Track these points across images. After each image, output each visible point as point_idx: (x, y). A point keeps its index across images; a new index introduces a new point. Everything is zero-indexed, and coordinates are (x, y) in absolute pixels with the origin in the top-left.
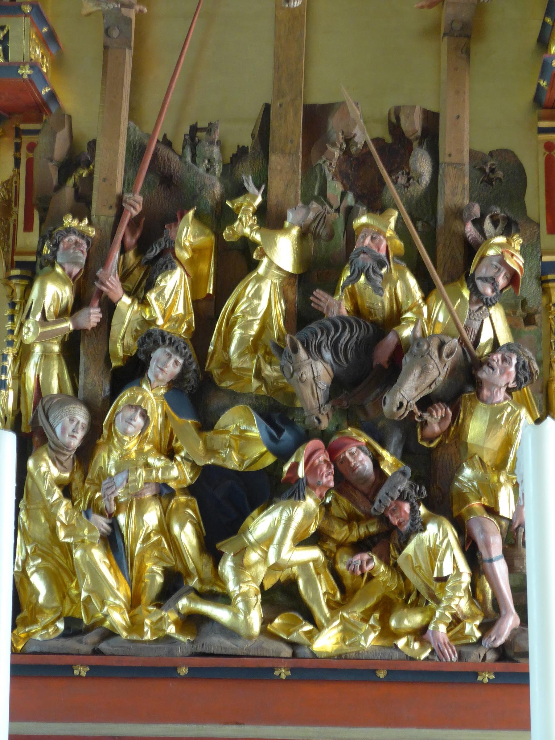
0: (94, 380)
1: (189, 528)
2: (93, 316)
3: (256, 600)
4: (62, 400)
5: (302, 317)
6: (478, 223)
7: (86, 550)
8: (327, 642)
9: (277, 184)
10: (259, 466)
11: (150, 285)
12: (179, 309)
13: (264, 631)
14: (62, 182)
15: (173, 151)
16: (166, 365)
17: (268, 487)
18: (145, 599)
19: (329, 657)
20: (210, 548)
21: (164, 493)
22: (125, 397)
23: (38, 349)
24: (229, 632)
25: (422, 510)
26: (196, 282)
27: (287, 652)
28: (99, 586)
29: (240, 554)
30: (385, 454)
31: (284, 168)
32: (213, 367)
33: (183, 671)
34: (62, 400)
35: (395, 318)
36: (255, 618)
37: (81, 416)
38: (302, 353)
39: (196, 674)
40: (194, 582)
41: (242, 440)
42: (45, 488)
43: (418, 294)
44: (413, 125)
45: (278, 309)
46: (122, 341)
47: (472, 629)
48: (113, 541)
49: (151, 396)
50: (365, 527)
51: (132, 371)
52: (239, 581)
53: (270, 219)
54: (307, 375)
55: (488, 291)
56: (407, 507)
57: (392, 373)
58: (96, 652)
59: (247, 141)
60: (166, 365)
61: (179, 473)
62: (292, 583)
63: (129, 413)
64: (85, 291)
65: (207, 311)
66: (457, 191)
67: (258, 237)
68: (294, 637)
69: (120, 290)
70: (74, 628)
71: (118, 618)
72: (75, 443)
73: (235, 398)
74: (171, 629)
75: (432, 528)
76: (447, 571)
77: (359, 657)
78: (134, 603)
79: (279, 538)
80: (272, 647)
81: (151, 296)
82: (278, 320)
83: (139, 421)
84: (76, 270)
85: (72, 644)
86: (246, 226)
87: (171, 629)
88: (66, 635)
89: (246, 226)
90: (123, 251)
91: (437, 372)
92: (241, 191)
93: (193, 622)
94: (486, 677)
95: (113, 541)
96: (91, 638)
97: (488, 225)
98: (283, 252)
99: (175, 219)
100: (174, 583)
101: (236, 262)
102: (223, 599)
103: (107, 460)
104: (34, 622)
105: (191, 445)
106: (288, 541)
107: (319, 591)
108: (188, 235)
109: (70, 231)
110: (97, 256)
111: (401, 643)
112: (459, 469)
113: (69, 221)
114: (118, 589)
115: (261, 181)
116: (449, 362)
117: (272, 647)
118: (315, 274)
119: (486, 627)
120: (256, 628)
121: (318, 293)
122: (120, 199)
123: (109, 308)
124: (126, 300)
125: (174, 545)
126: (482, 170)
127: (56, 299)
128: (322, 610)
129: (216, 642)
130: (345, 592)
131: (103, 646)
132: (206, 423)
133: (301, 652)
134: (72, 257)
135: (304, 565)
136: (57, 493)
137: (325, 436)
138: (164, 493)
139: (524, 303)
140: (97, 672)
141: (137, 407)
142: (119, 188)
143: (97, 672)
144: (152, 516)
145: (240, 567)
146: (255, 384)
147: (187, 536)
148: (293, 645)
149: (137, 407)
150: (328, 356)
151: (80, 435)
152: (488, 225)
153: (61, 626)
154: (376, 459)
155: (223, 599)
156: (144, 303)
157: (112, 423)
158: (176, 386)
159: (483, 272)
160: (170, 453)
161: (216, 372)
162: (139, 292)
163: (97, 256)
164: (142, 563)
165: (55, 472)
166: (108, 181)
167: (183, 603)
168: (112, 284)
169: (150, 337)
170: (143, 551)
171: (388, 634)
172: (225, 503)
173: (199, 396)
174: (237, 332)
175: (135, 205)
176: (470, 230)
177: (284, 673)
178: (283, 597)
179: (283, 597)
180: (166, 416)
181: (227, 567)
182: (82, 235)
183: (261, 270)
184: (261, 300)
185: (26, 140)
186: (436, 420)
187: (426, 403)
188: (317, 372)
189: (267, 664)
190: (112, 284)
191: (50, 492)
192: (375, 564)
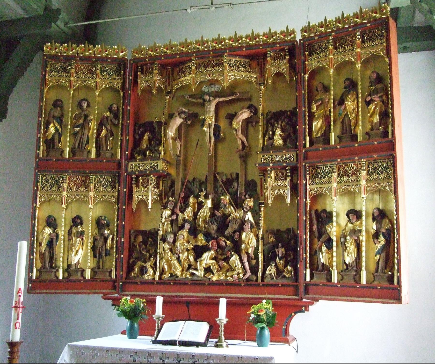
0: (176, 229)
1: (192, 257)
2: (174, 217)
3: (203, 270)
4: (170, 233)
5: (213, 215)
6: (245, 196)
7: (173, 261)
8: (215, 278)
9: (208, 189)
10: (204, 245)
11: (185, 210)
12: (191, 215)
13: (204, 276)
14: (170, 190)
15: (242, 140)
16: (187, 226)
17: (205, 249)
18: (185, 270)
19: (216, 281)
20: (196, 260)
21: (188, 250)
22: (180, 232)
23: (166, 223)
24: (198, 276)
25: (233, 253)
26: (194, 209)
27: (208, 280)
28: (175, 268)
29: (201, 261)
30: (228, 242)
31: (210, 187)
32: (197, 225)
33: (189, 283)
34: (170, 233)
35: (230, 215)
36: (203, 273)
37: (172, 236)
38: (210, 223)
39: (192, 284)
40: (193, 267)
41: (201, 240)
42: (166, 249)
43: (234, 211)
44: (234, 176)
45: (208, 215)
46: (180, 221)
47: (241, 275)
48: (178, 259)
49: (185, 232)
50: (222, 257)
51: (182, 227)
52: (200, 267)
53: (206, 197)
54: (212, 228)
55: (246, 210)
56: (230, 252)
57: (227, 226)
58: (175, 280)
59: (204, 180)
60: (187, 226)
61: (190, 246)
62: (210, 267)
63: (180, 235)
64: (173, 213)
65: (195, 214)
66: (241, 189)
67: (203, 201)
68: (209, 277)
69: (179, 212)
70: (172, 275)
71: (179, 273)
72: (172, 241)
73: (200, 231)
74: (188, 276)
75: (234, 256)
76: (236, 265)
77: (221, 280)
78: (183, 270)
79: (207, 258)
80: (205, 279)
81: (185, 213)
82: (208, 217)
83: (183, 237)
84: (171, 208)
85: (170, 278)
86: (202, 199)
87: (188, 276)
88: (170, 277)
89: (202, 199)
90: (181, 204)
91: (236, 227)
92: (202, 191)
93: (192, 274)
94: (243, 285)
95: (178, 259)
96: (174, 277)
97: (247, 196)
98: (209, 203)
99: (189, 197)
100: (190, 266)
101: (200, 205)
102: (196, 270)
103: (178, 244)
104: (166, 274)
105: (193, 242)
106: (208, 259)
107: (215, 269)
108: (191, 200)
109: (170, 201)
110: (175, 206)
111: (228, 278)
112: (242, 244)
113: (170, 199)
114: (179, 269)
115: (206, 189)
116: (238, 224)
117: (205, 279)
118: (216, 205)
119: (244, 275)
120: (202, 275)
121: (215, 211)
122: (180, 194)
123: (177, 215)
124: (180, 213)
125: (189, 260)
126: (248, 185)
127: (168, 214)
128: (215, 272)
129: (195, 278)
130: (221, 268)
131: (176, 279)
132: (196, 236)
133: (211, 280)
134: (170, 206)
135: (212, 264)
136: (169, 250)
137: (216, 239)
138: (188, 250)
139: (256, 211)
140: (175, 284)
141: (182, 234)
142: (179, 191)
143: (175, 284)
144: (186, 254)
145: (200, 264)
146: (204, 229)
147: (191, 258)
148: (209, 279)
149: (182, 234)
150: (216, 224)
151: (172, 239)
152: (247, 196)
153: (170, 275)
154: (226, 243)
155: (196, 270)
156: (183, 214)
157: (178, 237)
158: (190, 229)
159: (245, 207)
160: (188, 242)
161: (197, 227)
162: (182, 212)
163: (175, 206)
164: (184, 264)
165: (168, 247)
166: (177, 190)
167: (191, 271)
168: (178, 211)
169: (185, 220)
170: (184, 261)
171: (226, 276)
172: (198, 252)
173: (194, 232)
174: (201, 219)
175: (182, 195)
176: (243, 197)
177: (207, 284)
178: (208, 270)
179: (208, 270)
180: (188, 236)
181: (198, 264)
182: (173, 201)
183: (205, 207)
184: (205, 212)
185: (164, 182)
186: (237, 235)
187: (234, 232)
188: (214, 227)
189: (204, 282)
190: (178, 211)
191: (167, 250)
192: (224, 263)
